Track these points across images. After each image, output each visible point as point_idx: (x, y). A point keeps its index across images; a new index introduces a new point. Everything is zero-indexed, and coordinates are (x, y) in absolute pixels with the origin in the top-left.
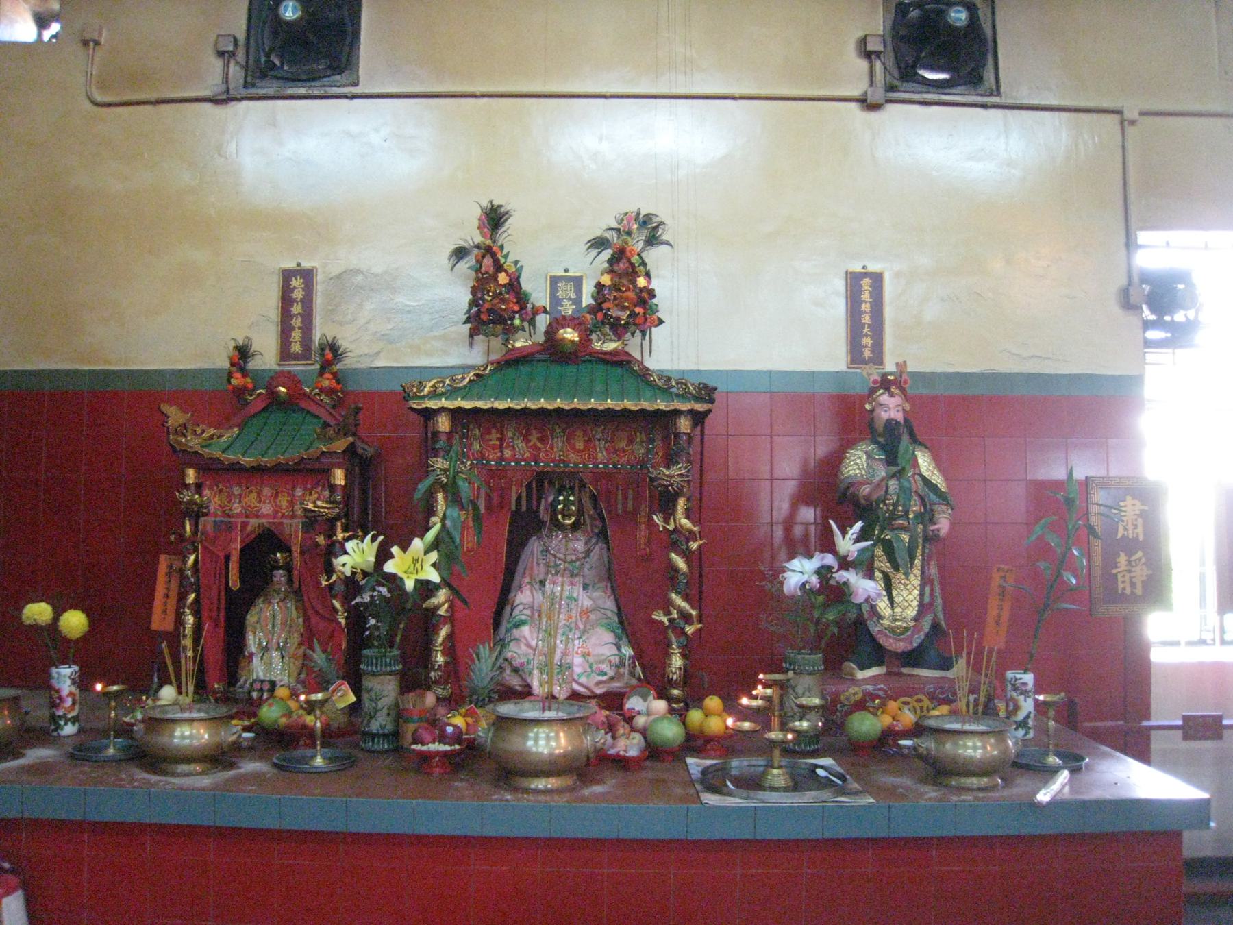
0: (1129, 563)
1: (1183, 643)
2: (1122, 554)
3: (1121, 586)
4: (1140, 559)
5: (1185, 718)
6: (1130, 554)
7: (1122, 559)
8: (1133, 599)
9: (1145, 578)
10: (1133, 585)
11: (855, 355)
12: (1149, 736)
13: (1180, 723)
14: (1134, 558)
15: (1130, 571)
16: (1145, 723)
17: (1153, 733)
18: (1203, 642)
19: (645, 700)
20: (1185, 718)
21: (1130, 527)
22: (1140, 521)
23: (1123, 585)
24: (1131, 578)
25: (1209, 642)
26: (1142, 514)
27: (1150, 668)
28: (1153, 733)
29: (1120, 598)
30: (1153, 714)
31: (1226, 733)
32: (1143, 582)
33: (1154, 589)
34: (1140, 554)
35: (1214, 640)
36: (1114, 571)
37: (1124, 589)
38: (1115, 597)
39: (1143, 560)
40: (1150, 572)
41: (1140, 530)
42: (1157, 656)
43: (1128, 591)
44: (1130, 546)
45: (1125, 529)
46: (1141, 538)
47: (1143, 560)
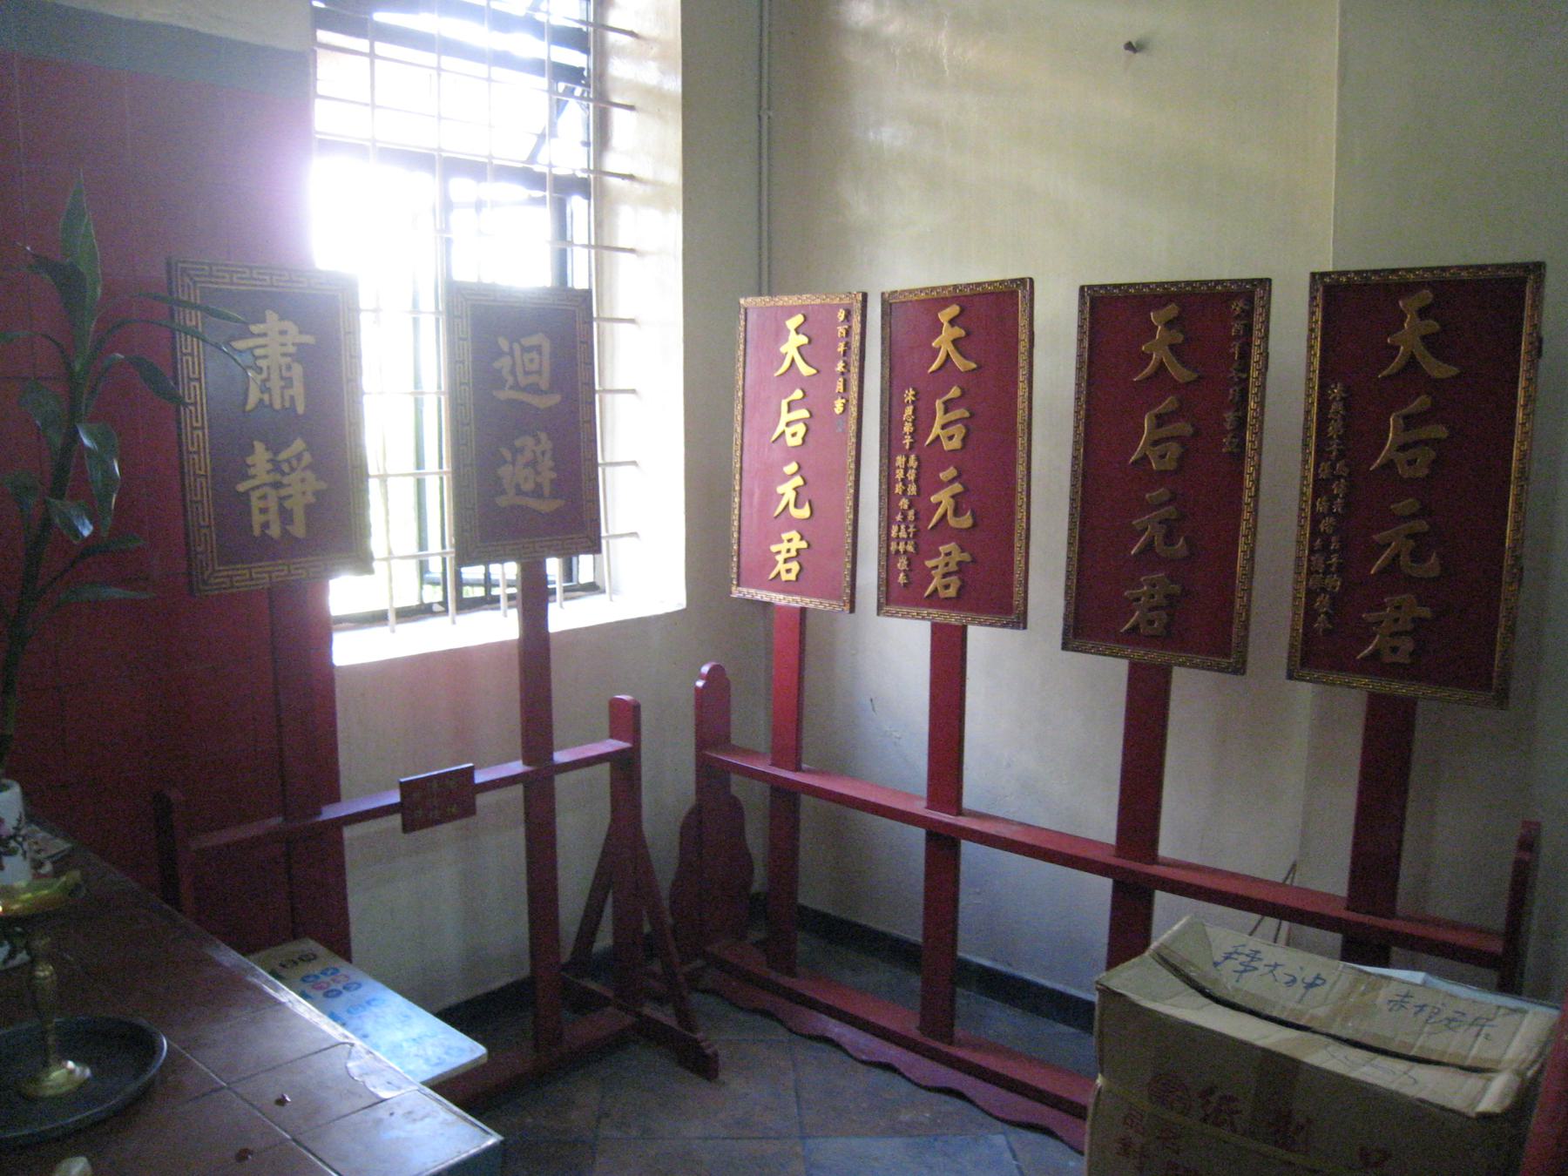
0: (276, 467)
1: (391, 617)
2: (259, 446)
3: (257, 519)
4: (299, 457)
5: (406, 788)
6: (274, 448)
7: (260, 457)
8: (290, 548)
9: (311, 499)
10: (286, 516)
11: (1165, 674)
12: (340, 840)
13: (395, 798)
14: (283, 456)
15: (277, 485)
16: (330, 812)
17: (348, 832)
18: (423, 611)
19: (663, 72)
20: (406, 788)
21: (276, 384)
22: (297, 370)
23: (263, 517)
24: (282, 499)
25: (437, 608)
26: (303, 354)
27: (332, 679)
28: (348, 832)
29: (266, 549)
30: (344, 782)
31: (482, 800)
32: (301, 332)
33: (336, 529)
34: (298, 445)
35: (444, 603)
36: (242, 487)
37: (266, 525)
38: (241, 542)
39: (307, 458)
40: (323, 485)
41: (298, 390)
42: (349, 651)
43: (275, 531)
44: (278, 428)
45: (264, 388)
46: (300, 409)
47: (307, 458)
